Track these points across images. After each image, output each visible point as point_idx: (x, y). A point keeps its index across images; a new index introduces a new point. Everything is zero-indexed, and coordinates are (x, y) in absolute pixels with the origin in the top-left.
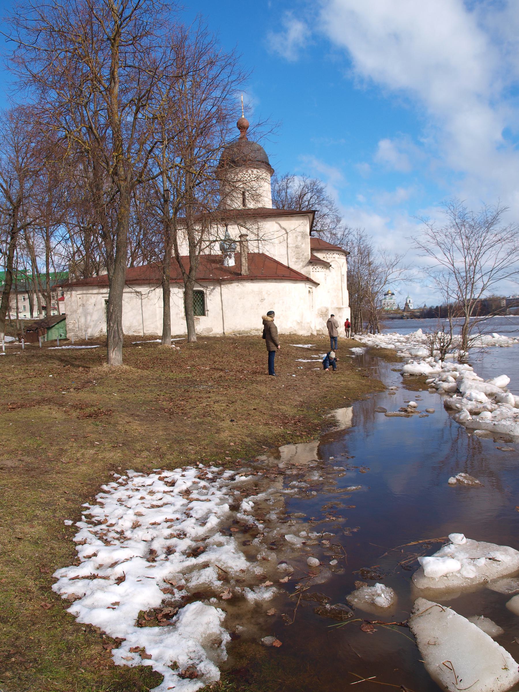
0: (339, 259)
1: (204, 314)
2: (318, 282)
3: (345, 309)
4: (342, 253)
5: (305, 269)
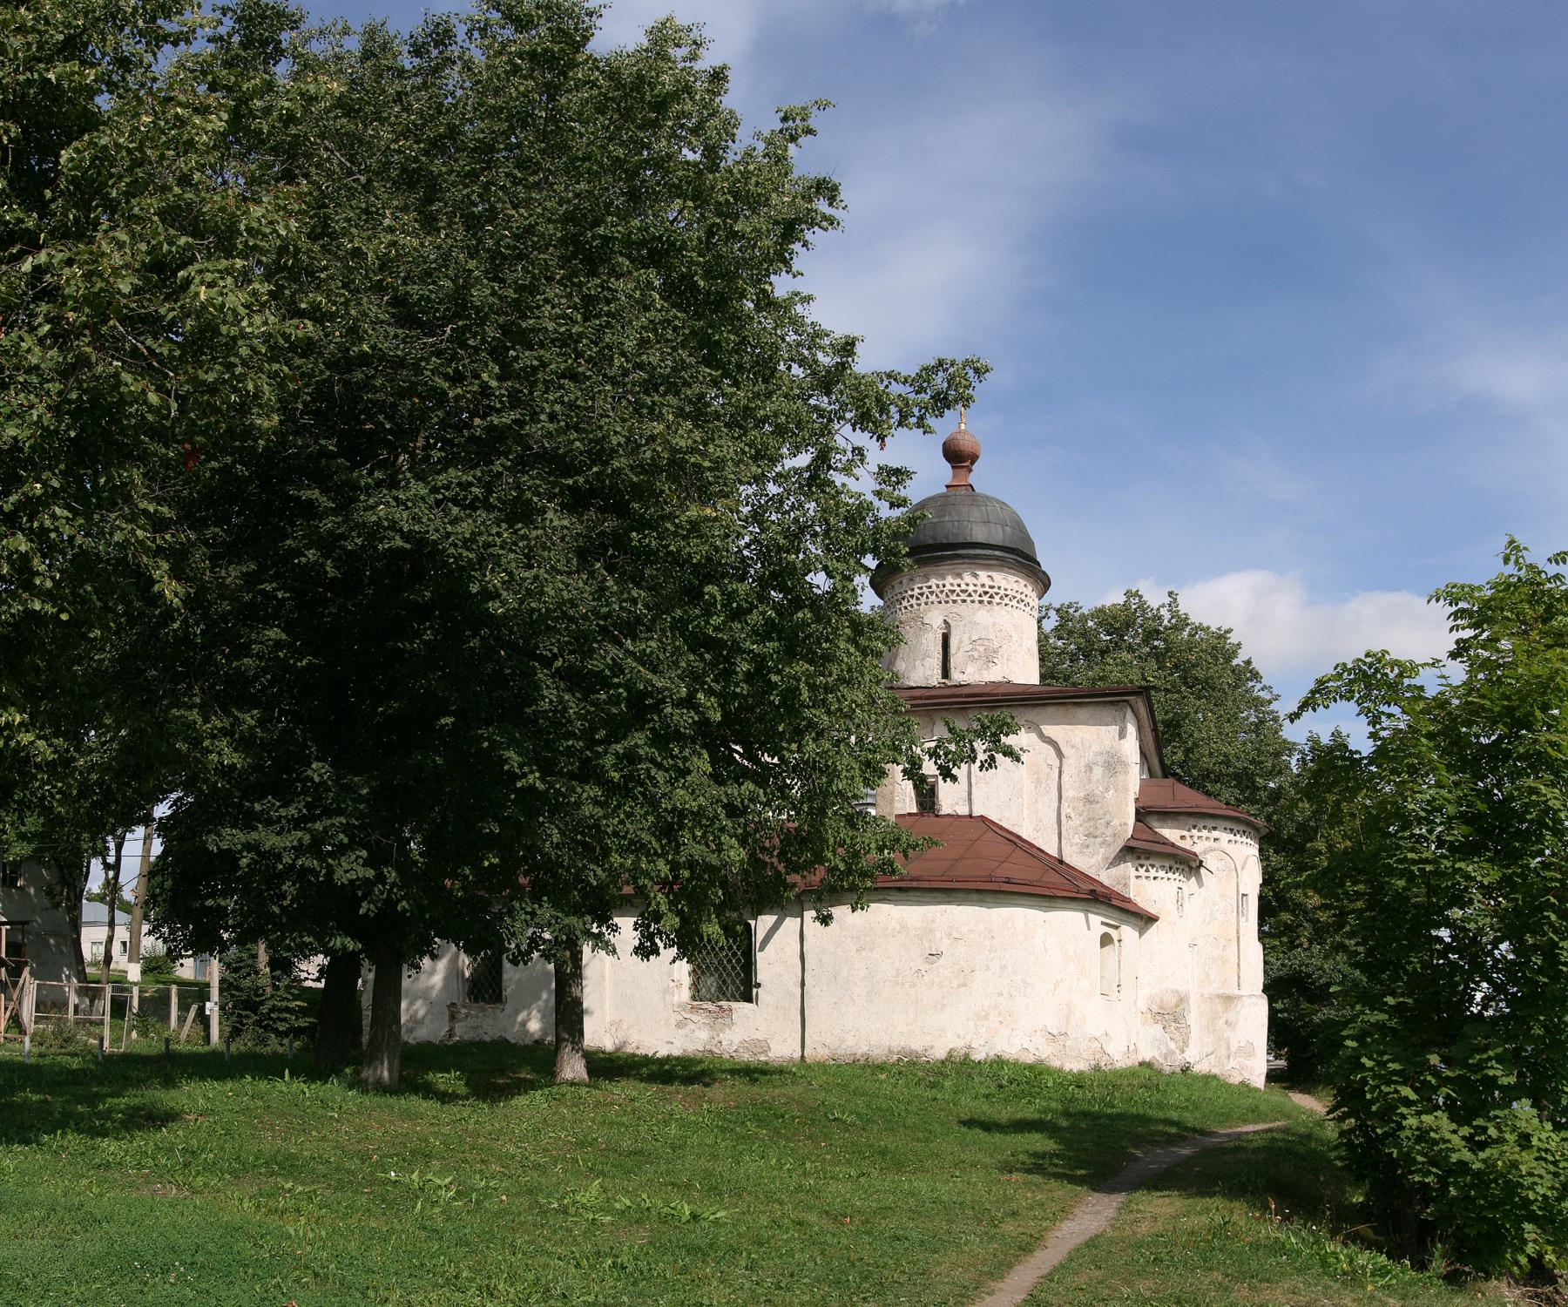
0: (1232, 845)
1: (748, 997)
2: (1152, 910)
3: (1247, 1001)
4: (1242, 828)
5: (1113, 870)
